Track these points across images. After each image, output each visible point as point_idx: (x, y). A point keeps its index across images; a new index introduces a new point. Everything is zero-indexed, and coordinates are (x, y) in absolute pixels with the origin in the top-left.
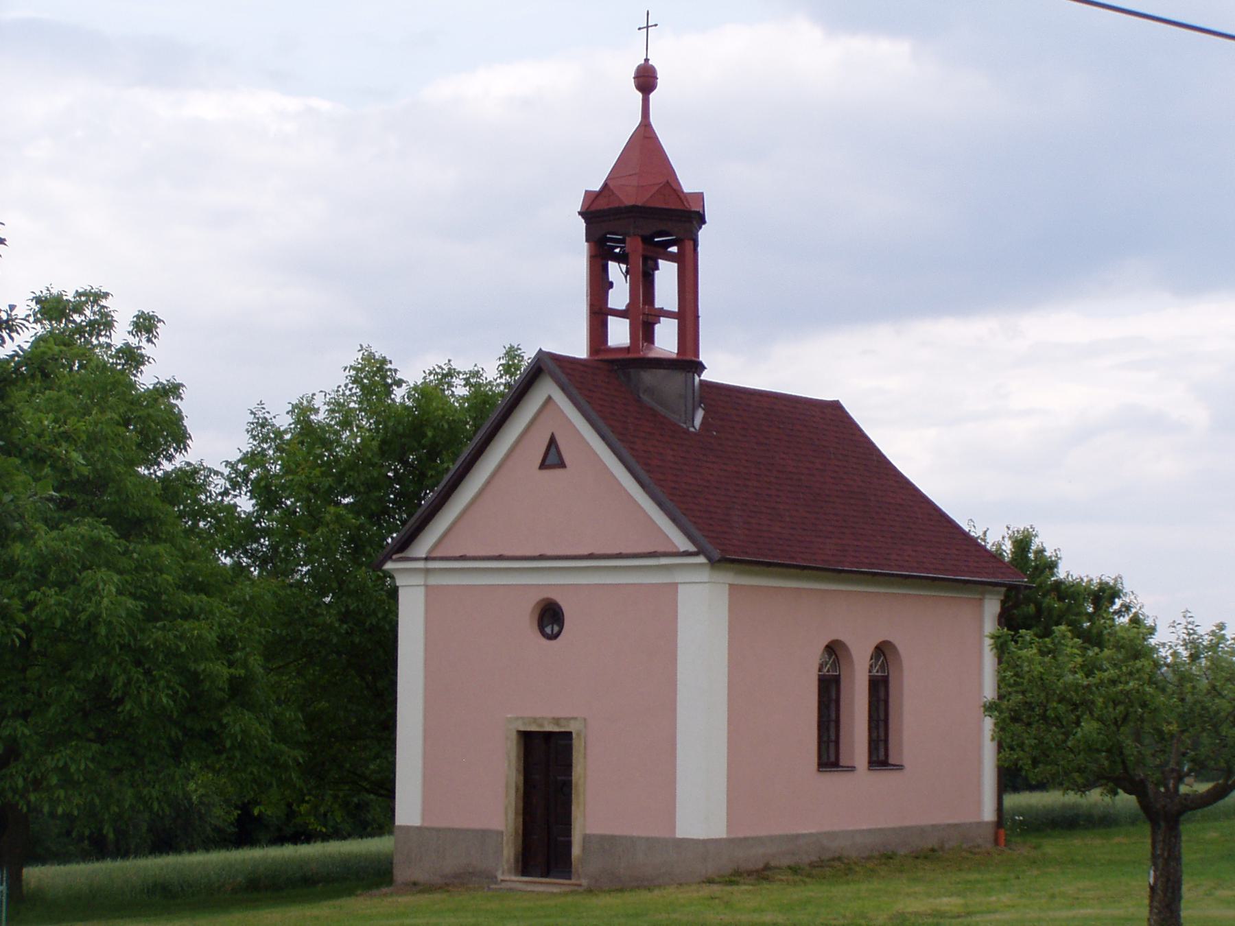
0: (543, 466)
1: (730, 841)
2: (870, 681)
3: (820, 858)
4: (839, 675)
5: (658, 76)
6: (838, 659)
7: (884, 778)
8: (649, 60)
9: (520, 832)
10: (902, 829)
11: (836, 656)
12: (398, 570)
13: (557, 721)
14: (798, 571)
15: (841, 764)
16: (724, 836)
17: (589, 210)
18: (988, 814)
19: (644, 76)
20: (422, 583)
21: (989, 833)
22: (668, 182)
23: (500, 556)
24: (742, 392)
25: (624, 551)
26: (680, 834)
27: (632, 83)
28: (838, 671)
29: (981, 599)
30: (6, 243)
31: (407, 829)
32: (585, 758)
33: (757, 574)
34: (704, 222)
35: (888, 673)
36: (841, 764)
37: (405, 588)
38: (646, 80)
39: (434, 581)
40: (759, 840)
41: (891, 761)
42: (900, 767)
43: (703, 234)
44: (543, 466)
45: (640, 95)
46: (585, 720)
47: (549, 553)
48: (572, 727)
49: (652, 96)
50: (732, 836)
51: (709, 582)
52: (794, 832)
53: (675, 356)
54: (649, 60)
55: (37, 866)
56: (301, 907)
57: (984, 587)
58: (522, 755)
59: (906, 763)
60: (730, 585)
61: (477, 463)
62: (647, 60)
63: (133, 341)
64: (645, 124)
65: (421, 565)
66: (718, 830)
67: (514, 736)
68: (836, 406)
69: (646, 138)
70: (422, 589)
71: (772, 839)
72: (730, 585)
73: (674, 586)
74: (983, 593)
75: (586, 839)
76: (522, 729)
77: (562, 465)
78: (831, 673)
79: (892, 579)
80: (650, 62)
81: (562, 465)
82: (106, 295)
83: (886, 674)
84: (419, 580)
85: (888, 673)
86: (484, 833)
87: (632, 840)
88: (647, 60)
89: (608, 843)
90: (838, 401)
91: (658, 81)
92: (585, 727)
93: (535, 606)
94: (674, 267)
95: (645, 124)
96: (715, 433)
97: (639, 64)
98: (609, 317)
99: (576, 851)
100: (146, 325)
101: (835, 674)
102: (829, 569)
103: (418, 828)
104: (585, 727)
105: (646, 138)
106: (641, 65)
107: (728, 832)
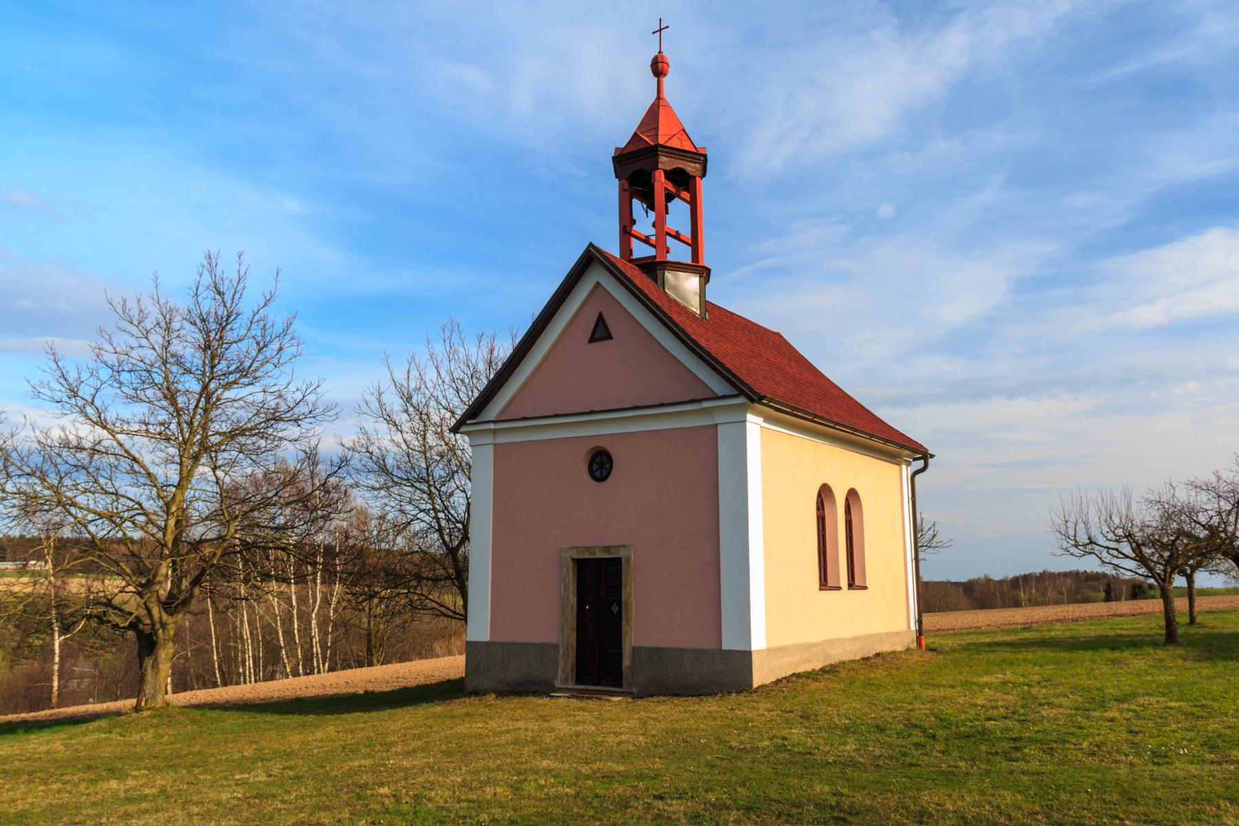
0: (592, 339)
13: (607, 549)
25: (639, 405)
38: (658, 68)
39: (502, 439)
44: (592, 339)
48: (622, 553)
65: (492, 426)
73: (716, 425)
75: (635, 650)
77: (609, 336)
81: (609, 336)
84: (489, 439)
87: (680, 652)
89: (656, 655)
99: (626, 662)
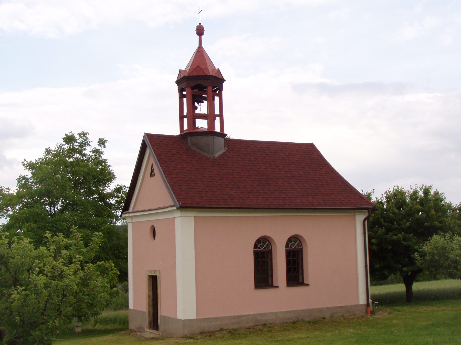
0: (151, 177)
1: (197, 320)
2: (254, 251)
3: (255, 324)
4: (271, 250)
6: (270, 243)
7: (296, 290)
8: (201, 24)
9: (152, 313)
10: (310, 310)
11: (300, 240)
12: (126, 217)
14: (275, 210)
16: (196, 318)
20: (131, 222)
22: (198, 66)
23: (136, 211)
26: (178, 318)
27: (195, 32)
28: (301, 247)
31: (131, 309)
32: (160, 286)
33: (216, 212)
35: (272, 248)
36: (274, 285)
37: (129, 223)
40: (217, 319)
45: (198, 37)
46: (160, 271)
47: (153, 208)
49: (202, 37)
50: (198, 318)
51: (180, 217)
52: (240, 314)
53: (207, 130)
54: (201, 24)
55: (386, 293)
56: (388, 310)
57: (355, 210)
58: (151, 284)
62: (200, 24)
63: (99, 147)
64: (200, 47)
68: (311, 146)
69: (200, 53)
70: (131, 223)
72: (194, 217)
76: (151, 274)
78: (297, 248)
79: (272, 210)
80: (201, 24)
82: (87, 134)
83: (271, 249)
85: (272, 248)
88: (200, 24)
93: (151, 228)
95: (200, 47)
96: (226, 158)
98: (196, 120)
101: (270, 249)
105: (200, 53)
106: (198, 26)
107: (197, 314)
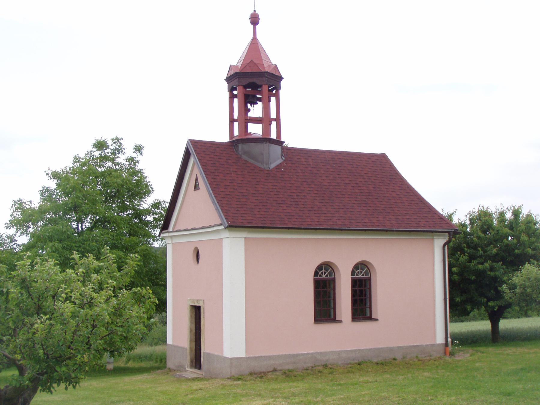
4: (335, 278)
5: (260, 17)
7: (363, 326)
15: (337, 319)
16: (245, 356)
17: (228, 76)
18: (440, 339)
19: (253, 18)
21: (442, 349)
24: (318, 152)
27: (248, 21)
29: (433, 239)
30: (252, 133)
31: (169, 345)
34: (281, 78)
36: (337, 319)
40: (270, 358)
41: (373, 317)
42: (376, 320)
43: (282, 83)
46: (204, 300)
49: (257, 26)
53: (261, 137)
59: (379, 317)
60: (245, 238)
61: (181, 190)
62: (255, 11)
63: (134, 155)
66: (242, 354)
67: (189, 306)
69: (254, 45)
71: (279, 357)
74: (433, 236)
80: (256, 12)
86: (183, 348)
90: (385, 153)
91: (260, 20)
92: (204, 304)
94: (274, 98)
97: (251, 13)
100: (139, 149)
102: (284, 227)
103: (171, 345)
104: (204, 304)
105: (254, 45)
